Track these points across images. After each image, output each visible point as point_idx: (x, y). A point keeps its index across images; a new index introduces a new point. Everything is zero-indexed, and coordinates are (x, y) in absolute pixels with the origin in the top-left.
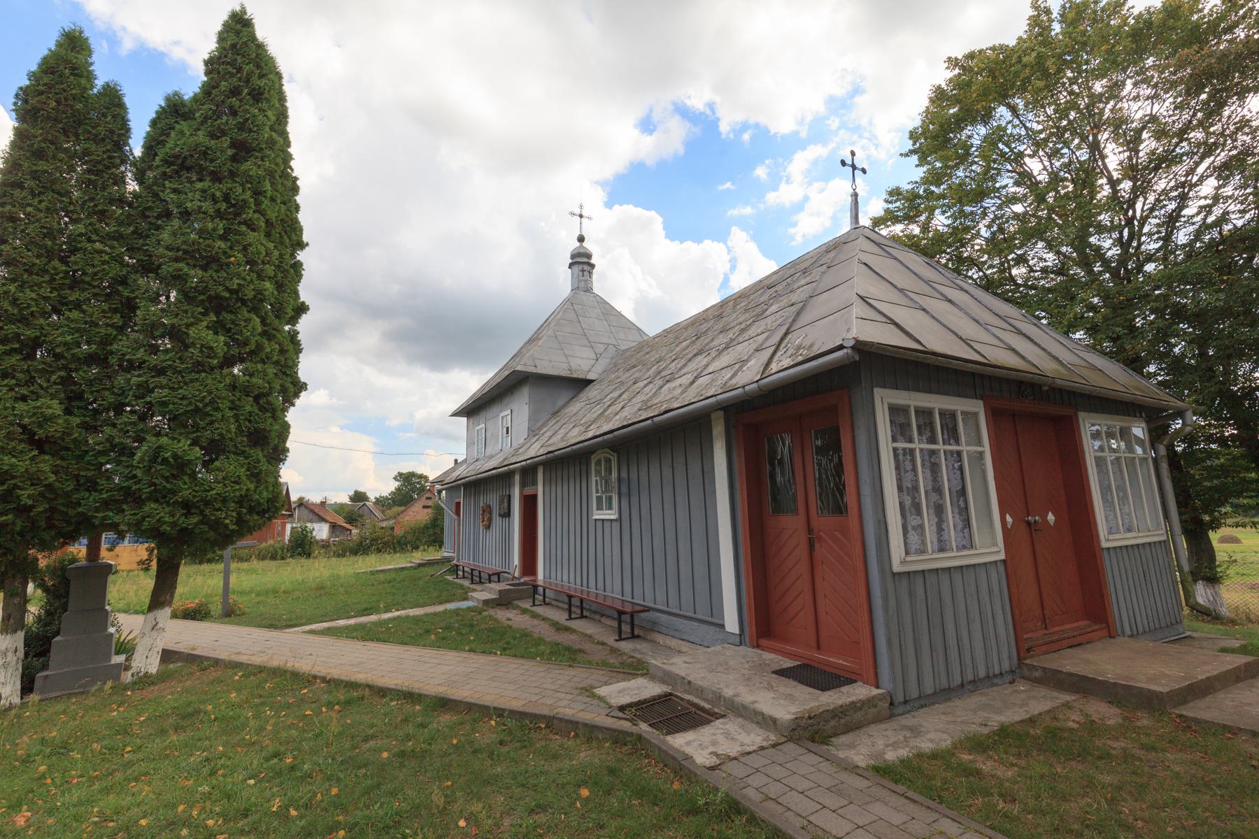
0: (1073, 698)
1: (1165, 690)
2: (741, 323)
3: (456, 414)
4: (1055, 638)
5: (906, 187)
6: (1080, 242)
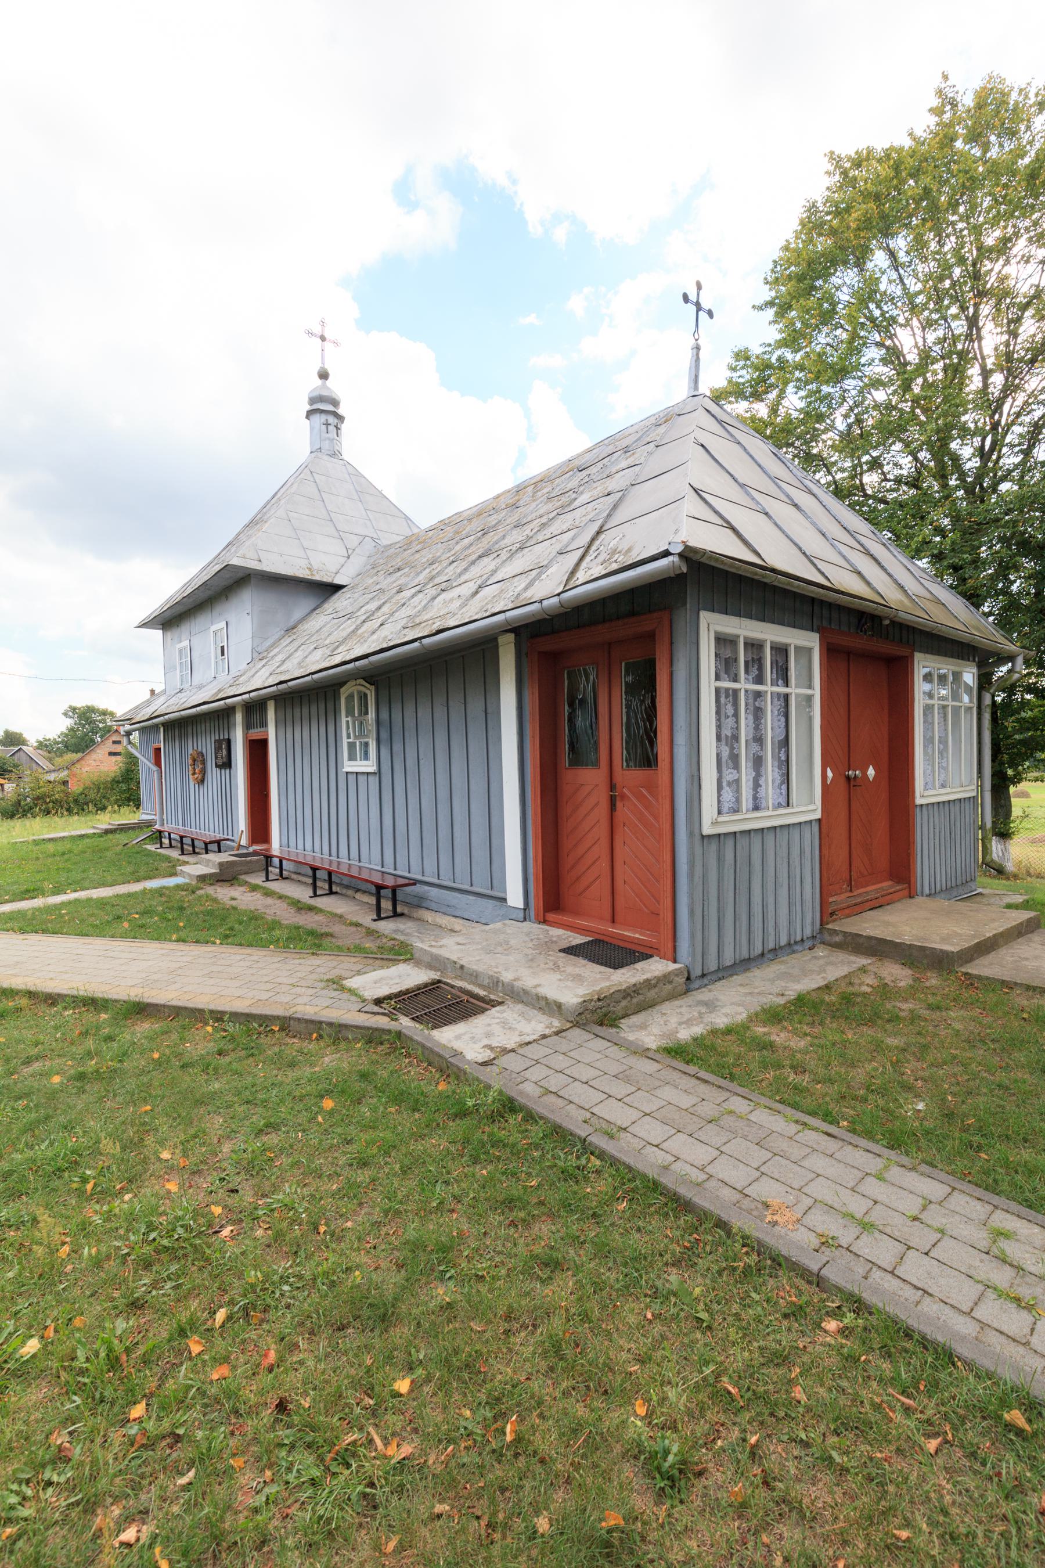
0: (869, 961)
1: (954, 949)
2: (541, 517)
3: (144, 625)
4: (859, 900)
5: (756, 350)
6: (940, 448)
